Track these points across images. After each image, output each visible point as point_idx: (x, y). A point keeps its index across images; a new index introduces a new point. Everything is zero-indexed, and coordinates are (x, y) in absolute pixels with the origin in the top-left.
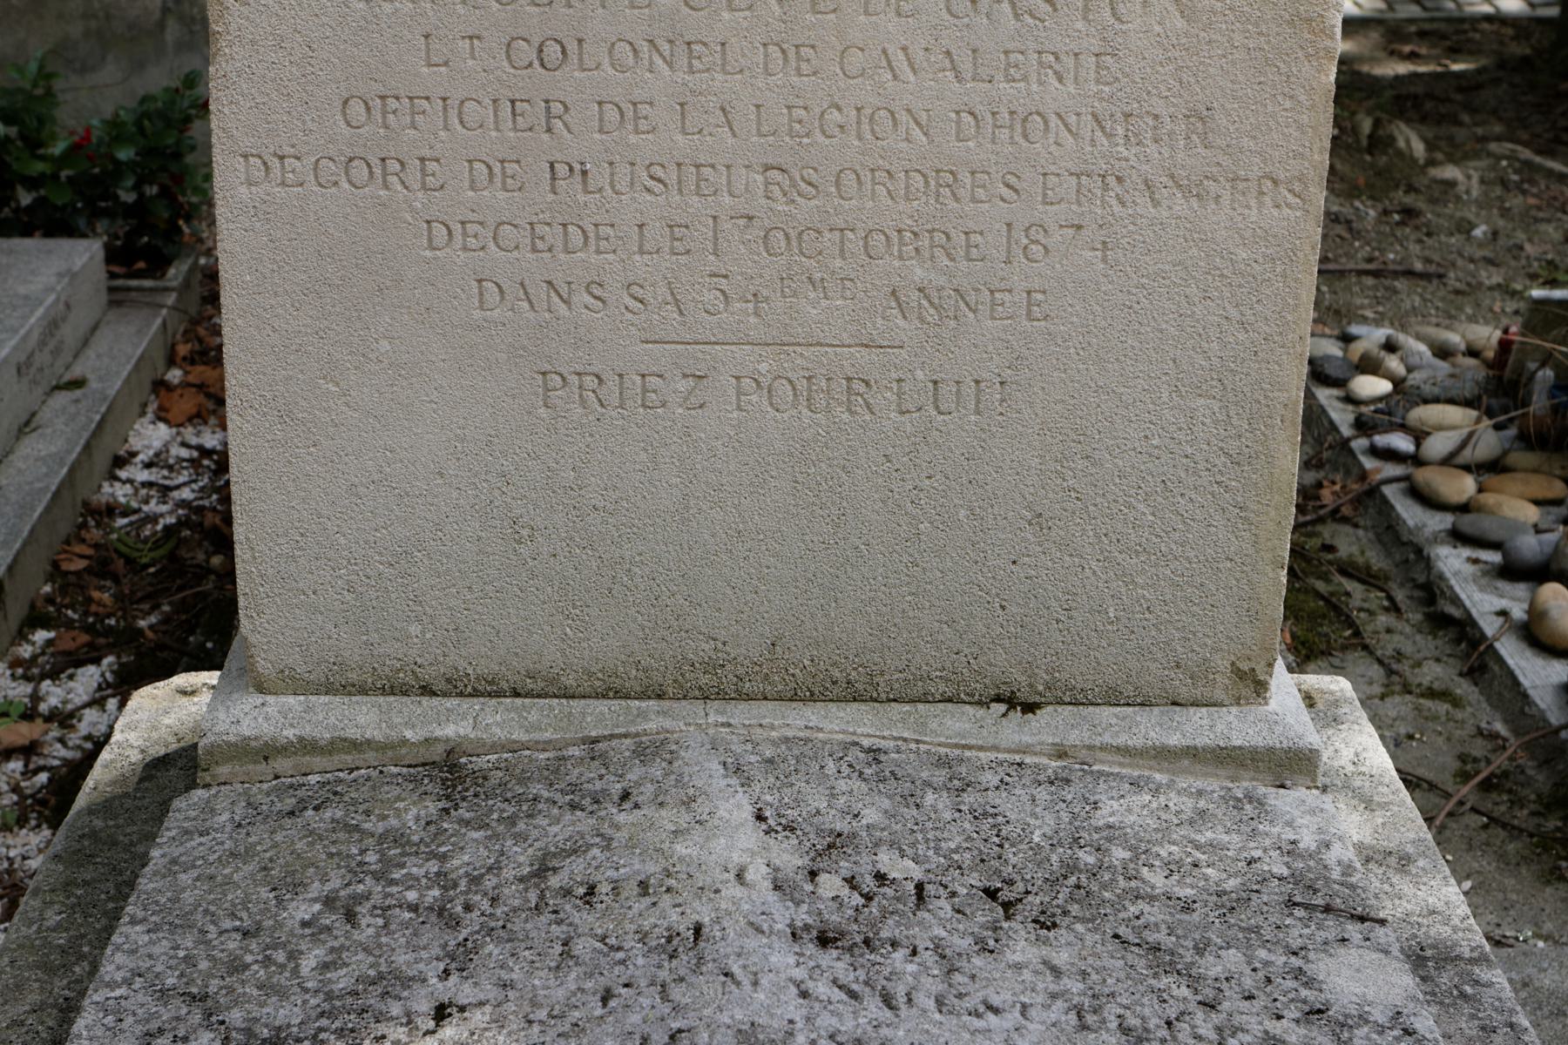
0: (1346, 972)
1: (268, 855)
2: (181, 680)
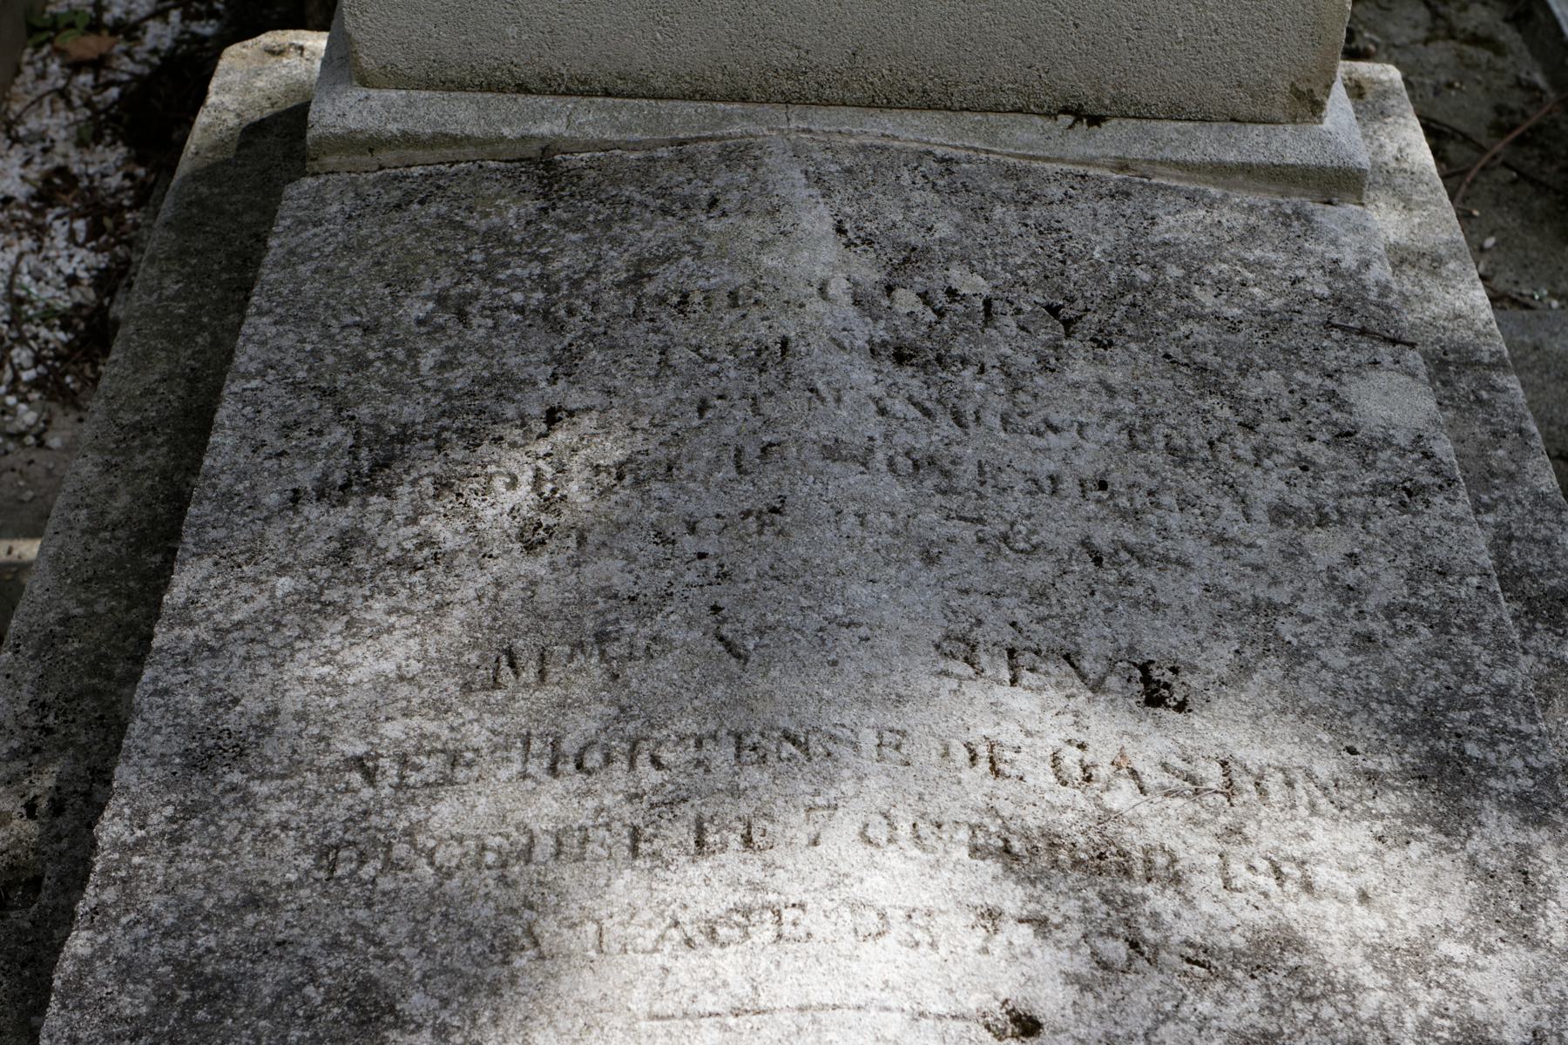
0: (1375, 395)
1: (380, 249)
2: (268, 39)
